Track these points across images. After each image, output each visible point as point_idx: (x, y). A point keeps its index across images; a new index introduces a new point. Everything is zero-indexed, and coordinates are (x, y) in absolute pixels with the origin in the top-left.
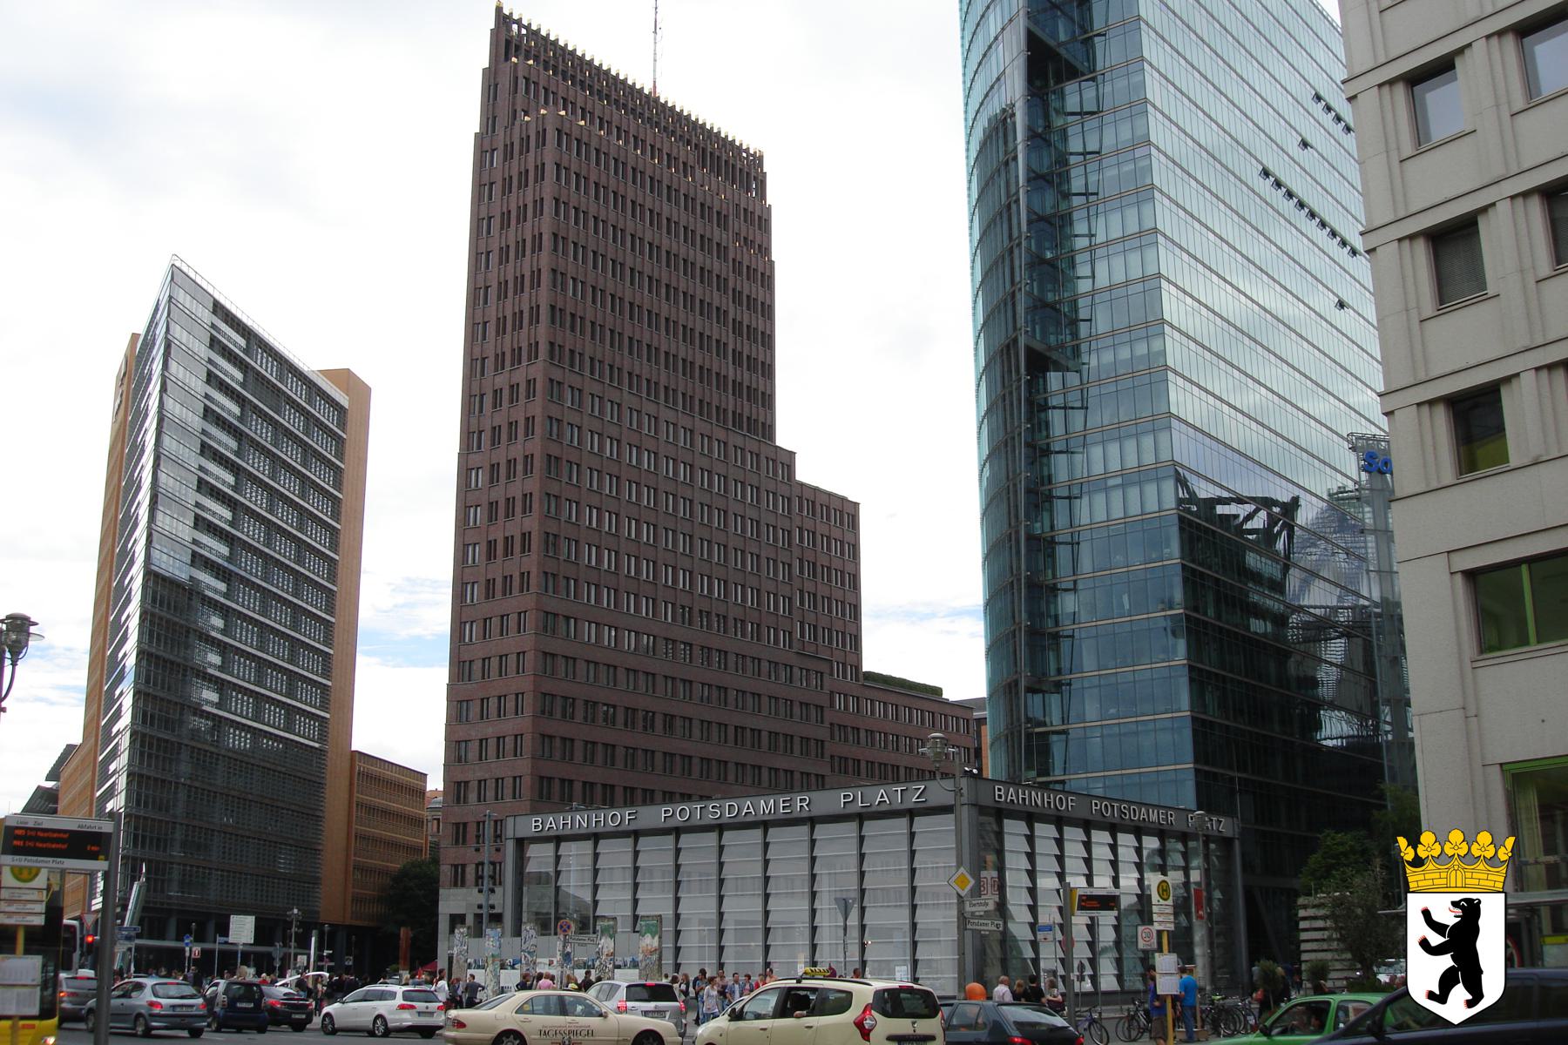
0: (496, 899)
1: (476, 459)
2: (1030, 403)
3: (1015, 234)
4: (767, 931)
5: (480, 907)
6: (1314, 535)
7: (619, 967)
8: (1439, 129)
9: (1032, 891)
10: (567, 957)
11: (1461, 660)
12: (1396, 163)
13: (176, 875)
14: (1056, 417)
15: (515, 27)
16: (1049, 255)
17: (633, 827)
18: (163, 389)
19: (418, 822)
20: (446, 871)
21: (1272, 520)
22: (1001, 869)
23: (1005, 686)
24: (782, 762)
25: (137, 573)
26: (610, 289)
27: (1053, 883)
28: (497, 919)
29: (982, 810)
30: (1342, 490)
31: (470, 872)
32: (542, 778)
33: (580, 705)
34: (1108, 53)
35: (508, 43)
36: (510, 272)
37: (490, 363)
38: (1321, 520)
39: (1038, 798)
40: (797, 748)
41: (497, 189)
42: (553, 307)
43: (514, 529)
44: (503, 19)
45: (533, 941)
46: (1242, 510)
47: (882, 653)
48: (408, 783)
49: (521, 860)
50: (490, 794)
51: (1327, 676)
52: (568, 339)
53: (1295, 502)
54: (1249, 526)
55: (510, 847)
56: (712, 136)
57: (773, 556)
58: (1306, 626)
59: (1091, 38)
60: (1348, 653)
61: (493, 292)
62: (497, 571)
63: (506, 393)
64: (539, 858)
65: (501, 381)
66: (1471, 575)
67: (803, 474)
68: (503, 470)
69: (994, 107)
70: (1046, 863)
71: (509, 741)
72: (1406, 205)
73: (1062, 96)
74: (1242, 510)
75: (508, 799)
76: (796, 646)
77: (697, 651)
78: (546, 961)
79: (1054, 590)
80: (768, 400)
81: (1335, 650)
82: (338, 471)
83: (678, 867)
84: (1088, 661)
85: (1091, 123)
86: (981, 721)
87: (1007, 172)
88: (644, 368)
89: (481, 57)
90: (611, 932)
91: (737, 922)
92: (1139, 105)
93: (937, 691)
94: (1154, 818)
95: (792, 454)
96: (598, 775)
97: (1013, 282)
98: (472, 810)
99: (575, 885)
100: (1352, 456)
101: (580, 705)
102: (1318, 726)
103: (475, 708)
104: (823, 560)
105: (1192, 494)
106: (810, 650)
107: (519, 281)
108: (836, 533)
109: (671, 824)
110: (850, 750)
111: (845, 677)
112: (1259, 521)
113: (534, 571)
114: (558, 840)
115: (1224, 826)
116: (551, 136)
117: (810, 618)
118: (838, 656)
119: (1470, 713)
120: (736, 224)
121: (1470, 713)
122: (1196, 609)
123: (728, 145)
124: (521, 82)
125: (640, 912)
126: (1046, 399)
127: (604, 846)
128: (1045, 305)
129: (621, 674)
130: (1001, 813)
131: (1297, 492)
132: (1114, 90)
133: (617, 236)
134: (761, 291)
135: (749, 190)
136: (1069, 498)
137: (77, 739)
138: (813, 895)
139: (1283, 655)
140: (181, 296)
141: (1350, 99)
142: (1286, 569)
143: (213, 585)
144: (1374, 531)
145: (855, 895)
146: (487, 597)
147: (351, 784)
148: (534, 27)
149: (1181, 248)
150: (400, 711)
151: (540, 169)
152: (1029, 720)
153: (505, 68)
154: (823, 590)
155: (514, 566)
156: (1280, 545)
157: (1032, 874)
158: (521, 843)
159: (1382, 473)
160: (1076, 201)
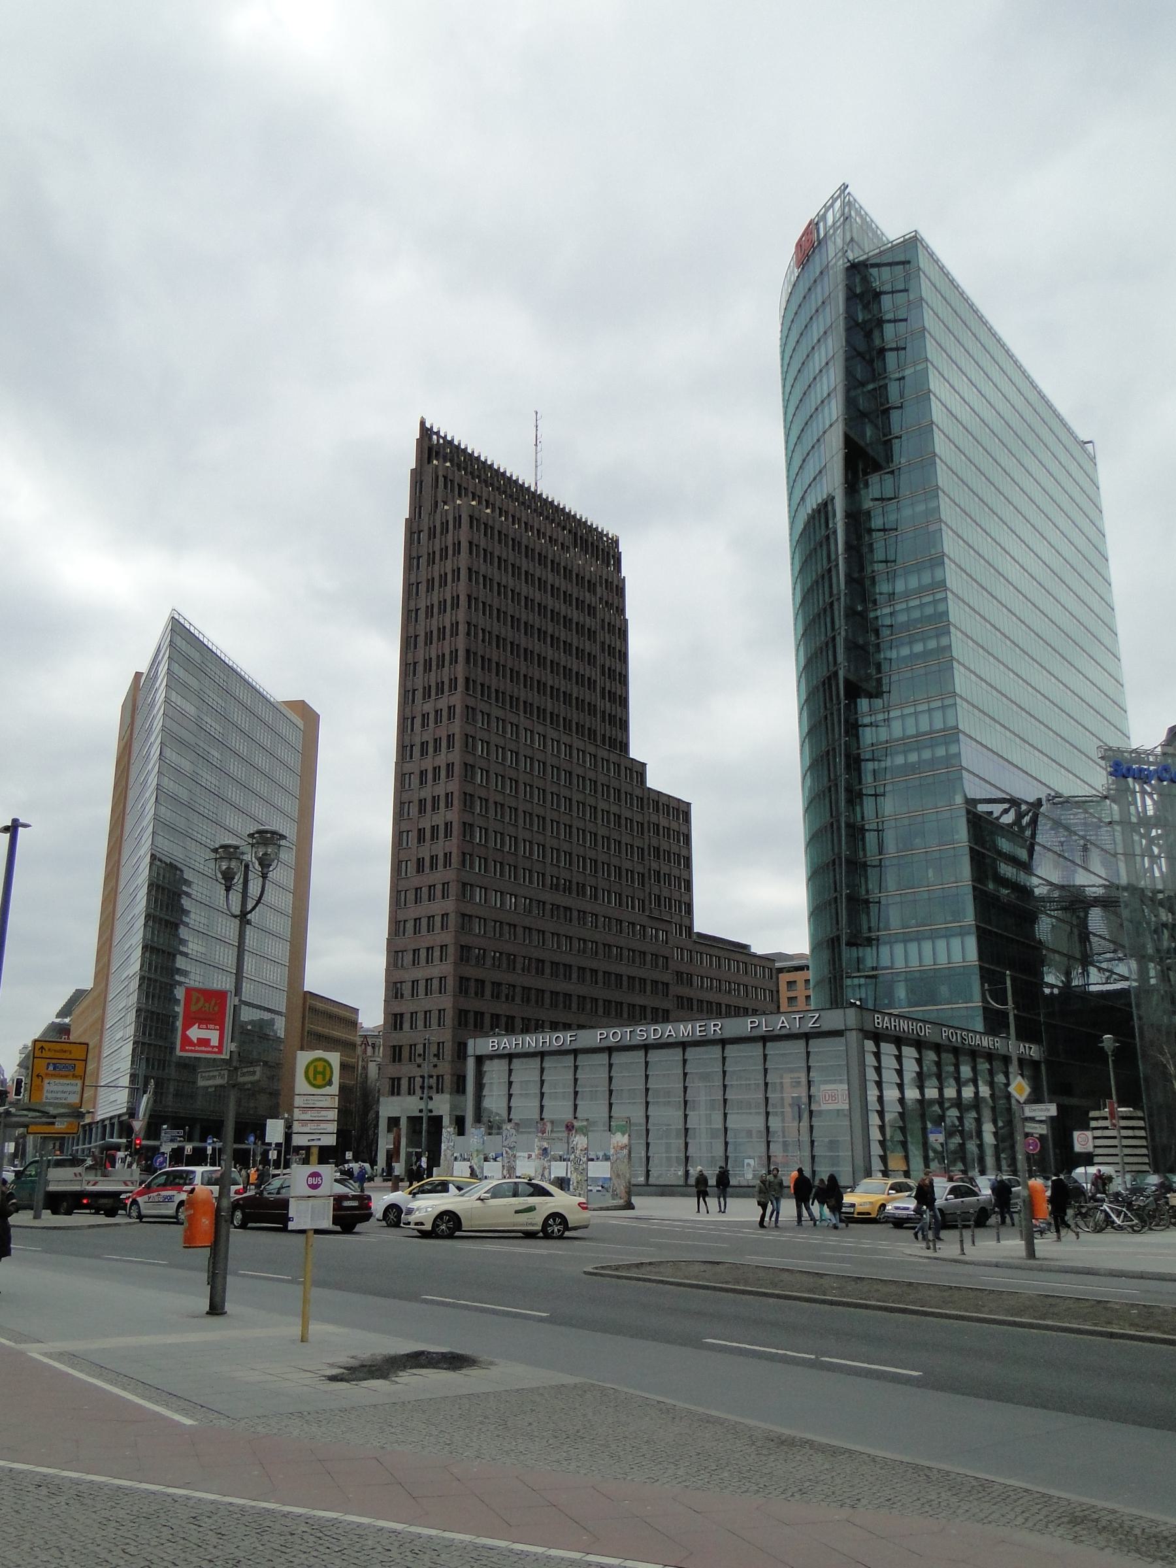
3: (835, 591)
5: (421, 1111)
7: (592, 1160)
9: (880, 1099)
15: (435, 437)
16: (859, 608)
17: (574, 1046)
21: (1020, 816)
24: (639, 1000)
27: (896, 1094)
31: (404, 1083)
34: (903, 454)
35: (430, 449)
36: (434, 624)
40: (649, 988)
41: (423, 561)
42: (468, 651)
43: (439, 819)
44: (426, 432)
45: (513, 1139)
46: (997, 809)
49: (479, 1075)
50: (420, 1023)
52: (479, 676)
55: (471, 1063)
56: (581, 524)
57: (582, 853)
59: (890, 440)
61: (421, 640)
62: (425, 852)
63: (432, 717)
64: (495, 1072)
70: (890, 1076)
71: (436, 983)
73: (867, 485)
75: (435, 1026)
78: (526, 1155)
80: (624, 725)
85: (892, 506)
87: (828, 545)
88: (536, 699)
92: (933, 492)
94: (985, 1044)
96: (502, 1008)
97: (833, 629)
98: (405, 1037)
103: (409, 957)
106: (656, 914)
107: (442, 631)
109: (605, 1044)
111: (681, 935)
112: (1008, 819)
113: (455, 851)
115: (1034, 1051)
118: (676, 919)
123: (591, 529)
124: (441, 479)
126: (857, 719)
129: (520, 931)
133: (509, 595)
134: (618, 643)
135: (608, 565)
136: (876, 795)
137: (88, 985)
144: (1120, 823)
145: (805, 1100)
146: (418, 872)
147: (304, 1018)
148: (449, 438)
149: (963, 601)
150: (349, 957)
151: (457, 546)
153: (429, 469)
155: (439, 848)
159: (1125, 777)
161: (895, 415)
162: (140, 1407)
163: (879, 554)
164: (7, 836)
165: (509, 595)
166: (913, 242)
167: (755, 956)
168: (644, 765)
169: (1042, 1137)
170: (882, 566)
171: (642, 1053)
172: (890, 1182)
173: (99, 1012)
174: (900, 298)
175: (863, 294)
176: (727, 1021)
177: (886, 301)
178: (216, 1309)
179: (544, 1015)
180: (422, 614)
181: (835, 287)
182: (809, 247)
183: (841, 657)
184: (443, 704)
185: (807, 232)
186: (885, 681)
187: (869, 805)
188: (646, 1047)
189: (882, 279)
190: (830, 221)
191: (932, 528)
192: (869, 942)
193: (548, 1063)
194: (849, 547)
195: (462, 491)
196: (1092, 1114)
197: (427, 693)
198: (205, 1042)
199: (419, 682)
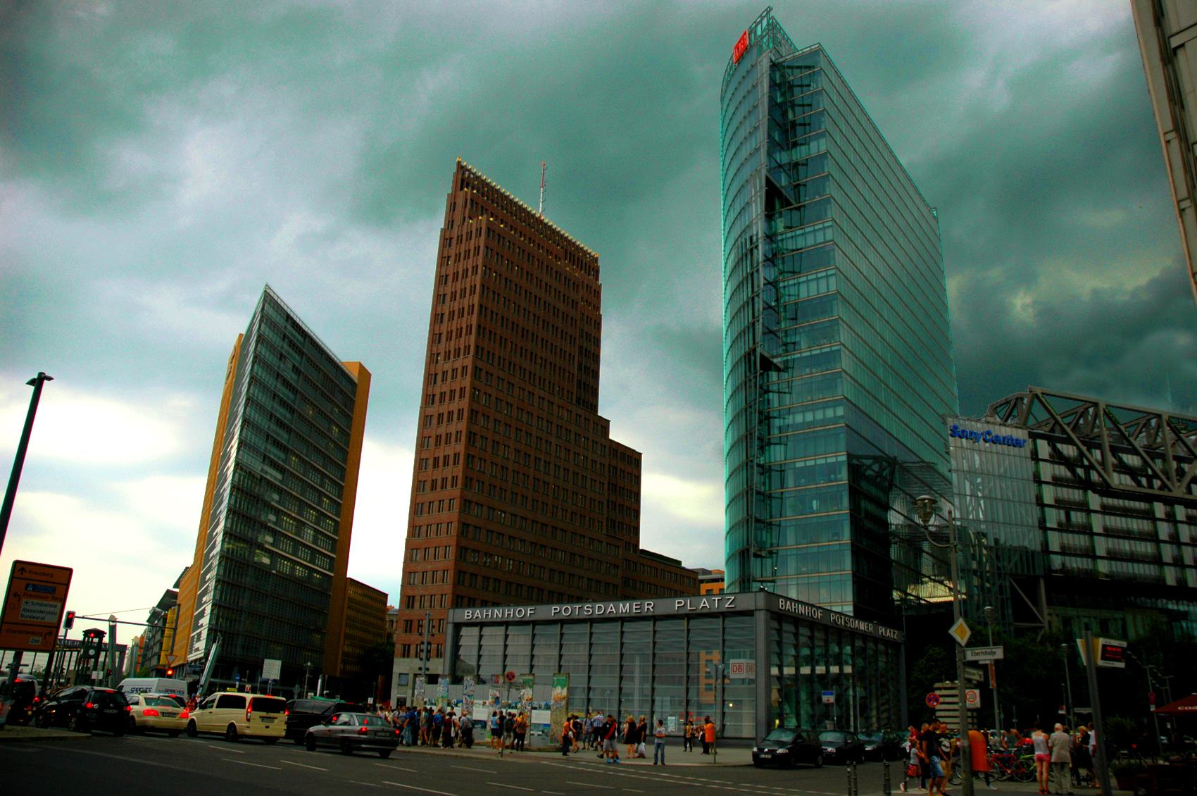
1: (432, 410)
14: (774, 397)
17: (533, 618)
25: (231, 464)
32: (458, 596)
35: (463, 181)
36: (456, 306)
44: (461, 168)
50: (427, 604)
55: (450, 629)
64: (469, 637)
67: (614, 436)
82: (341, 487)
84: (791, 538)
89: (455, 170)
93: (680, 562)
98: (416, 613)
113: (460, 475)
125: (592, 685)
128: (771, 332)
143: (274, 475)
150: (377, 551)
158: (458, 627)
164: (32, 388)
166: (817, 52)
167: (684, 569)
168: (608, 422)
177: (797, 90)
180: (448, 298)
182: (743, 50)
184: (458, 365)
190: (759, 33)
195: (483, 210)
197: (447, 356)
199: (442, 348)
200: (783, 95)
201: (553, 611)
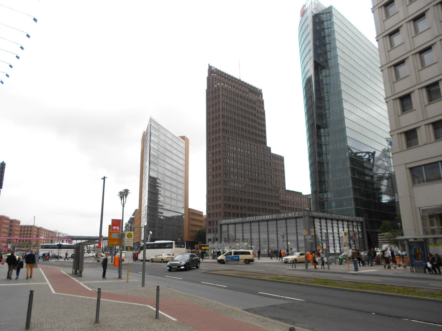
0: (217, 236)
2: (317, 135)
4: (268, 241)
6: (379, 159)
8: (402, 75)
10: (230, 247)
11: (409, 186)
12: (392, 84)
13: (157, 232)
14: (323, 138)
18: (150, 142)
19: (201, 221)
20: (207, 231)
21: (370, 156)
22: (315, 228)
23: (314, 192)
26: (241, 134)
27: (325, 231)
28: (217, 239)
29: (310, 217)
30: (385, 149)
33: (231, 198)
34: (331, 63)
35: (211, 71)
37: (211, 134)
38: (380, 155)
39: (321, 214)
42: (223, 122)
43: (217, 165)
44: (210, 67)
47: (289, 186)
48: (199, 214)
49: (221, 228)
50: (215, 215)
51: (384, 188)
53: (375, 152)
54: (364, 158)
58: (378, 177)
60: (388, 183)
64: (224, 228)
65: (214, 137)
66: (411, 169)
67: (272, 152)
68: (215, 154)
69: (308, 76)
70: (324, 227)
72: (394, 92)
73: (322, 73)
74: (363, 155)
76: (273, 185)
77: (253, 187)
79: (324, 172)
81: (385, 182)
83: (251, 229)
85: (328, 78)
86: (310, 199)
89: (208, 68)
90: (238, 242)
91: (263, 239)
93: (301, 193)
94: (346, 218)
95: (270, 148)
98: (212, 219)
99: (232, 233)
100: (387, 142)
101: (231, 198)
102: (381, 198)
104: (277, 168)
105: (352, 151)
106: (276, 186)
107: (216, 117)
108: (280, 163)
110: (284, 205)
112: (367, 156)
114: (228, 224)
115: (361, 219)
116: (221, 89)
117: (275, 180)
119: (412, 197)
120: (258, 103)
121: (412, 197)
122: (353, 175)
124: (214, 79)
125: (244, 238)
127: (237, 226)
130: (314, 218)
131: (375, 150)
132: (332, 71)
133: (233, 109)
138: (277, 234)
139: (373, 184)
140: (153, 124)
141: (382, 71)
142: (373, 166)
150: (198, 201)
152: (320, 198)
154: (277, 174)
156: (372, 161)
157: (321, 229)
160: (326, 94)
161: (329, 54)
162: (43, 276)
163: (325, 91)
165: (233, 109)
166: (331, 8)
169: (311, 243)
170: (326, 94)
171: (266, 222)
172: (299, 253)
173: (140, 215)
174: (329, 22)
175: (319, 22)
176: (277, 215)
177: (325, 23)
178: (120, 277)
179: (248, 212)
180: (211, 113)
181: (310, 22)
183: (315, 119)
184: (217, 136)
185: (303, 8)
186: (328, 124)
187: (324, 156)
188: (259, 221)
189: (324, 17)
191: (338, 83)
192: (325, 192)
193: (261, 223)
194: (316, 90)
196: (379, 234)
198: (116, 229)
200: (320, 26)
201: (248, 219)
